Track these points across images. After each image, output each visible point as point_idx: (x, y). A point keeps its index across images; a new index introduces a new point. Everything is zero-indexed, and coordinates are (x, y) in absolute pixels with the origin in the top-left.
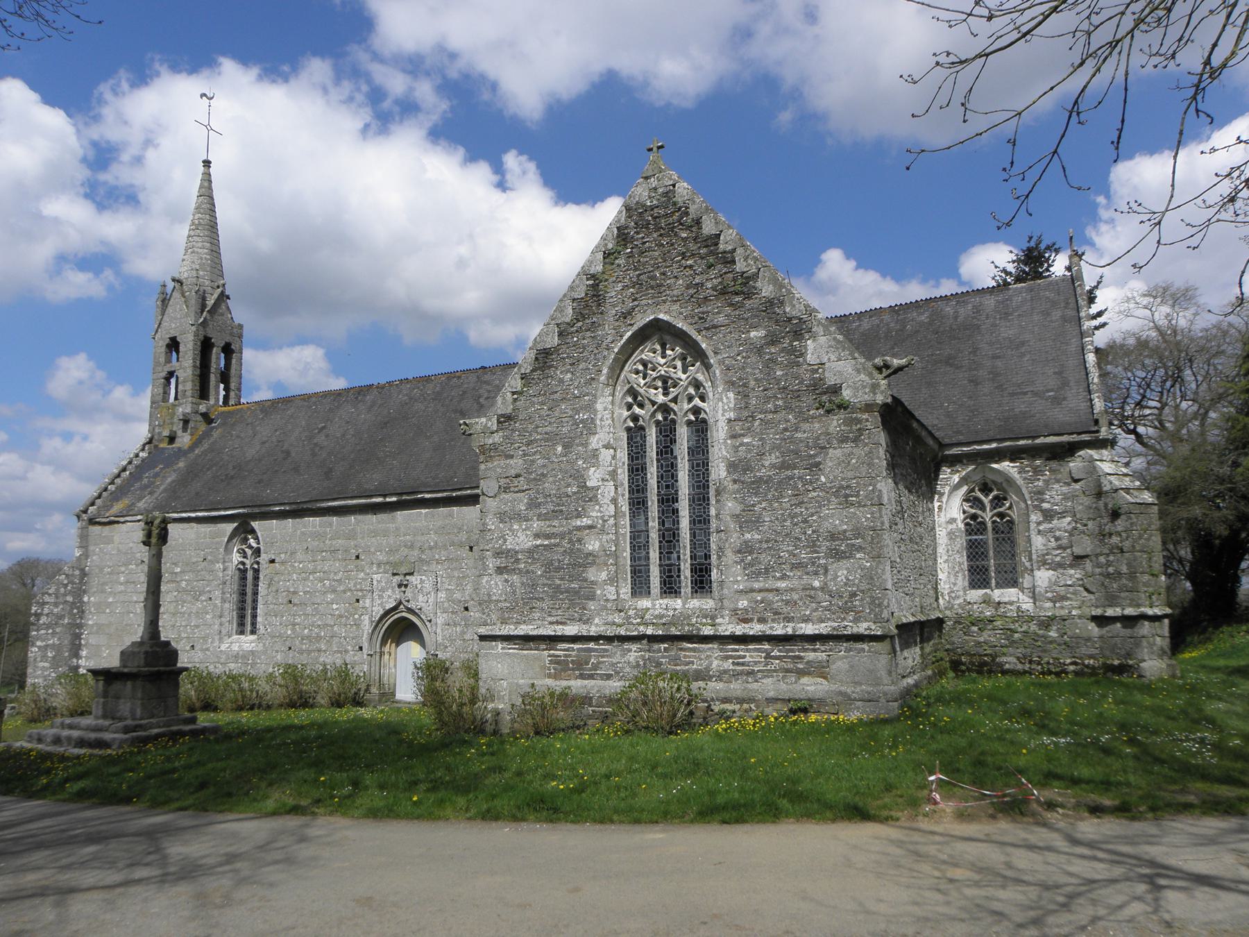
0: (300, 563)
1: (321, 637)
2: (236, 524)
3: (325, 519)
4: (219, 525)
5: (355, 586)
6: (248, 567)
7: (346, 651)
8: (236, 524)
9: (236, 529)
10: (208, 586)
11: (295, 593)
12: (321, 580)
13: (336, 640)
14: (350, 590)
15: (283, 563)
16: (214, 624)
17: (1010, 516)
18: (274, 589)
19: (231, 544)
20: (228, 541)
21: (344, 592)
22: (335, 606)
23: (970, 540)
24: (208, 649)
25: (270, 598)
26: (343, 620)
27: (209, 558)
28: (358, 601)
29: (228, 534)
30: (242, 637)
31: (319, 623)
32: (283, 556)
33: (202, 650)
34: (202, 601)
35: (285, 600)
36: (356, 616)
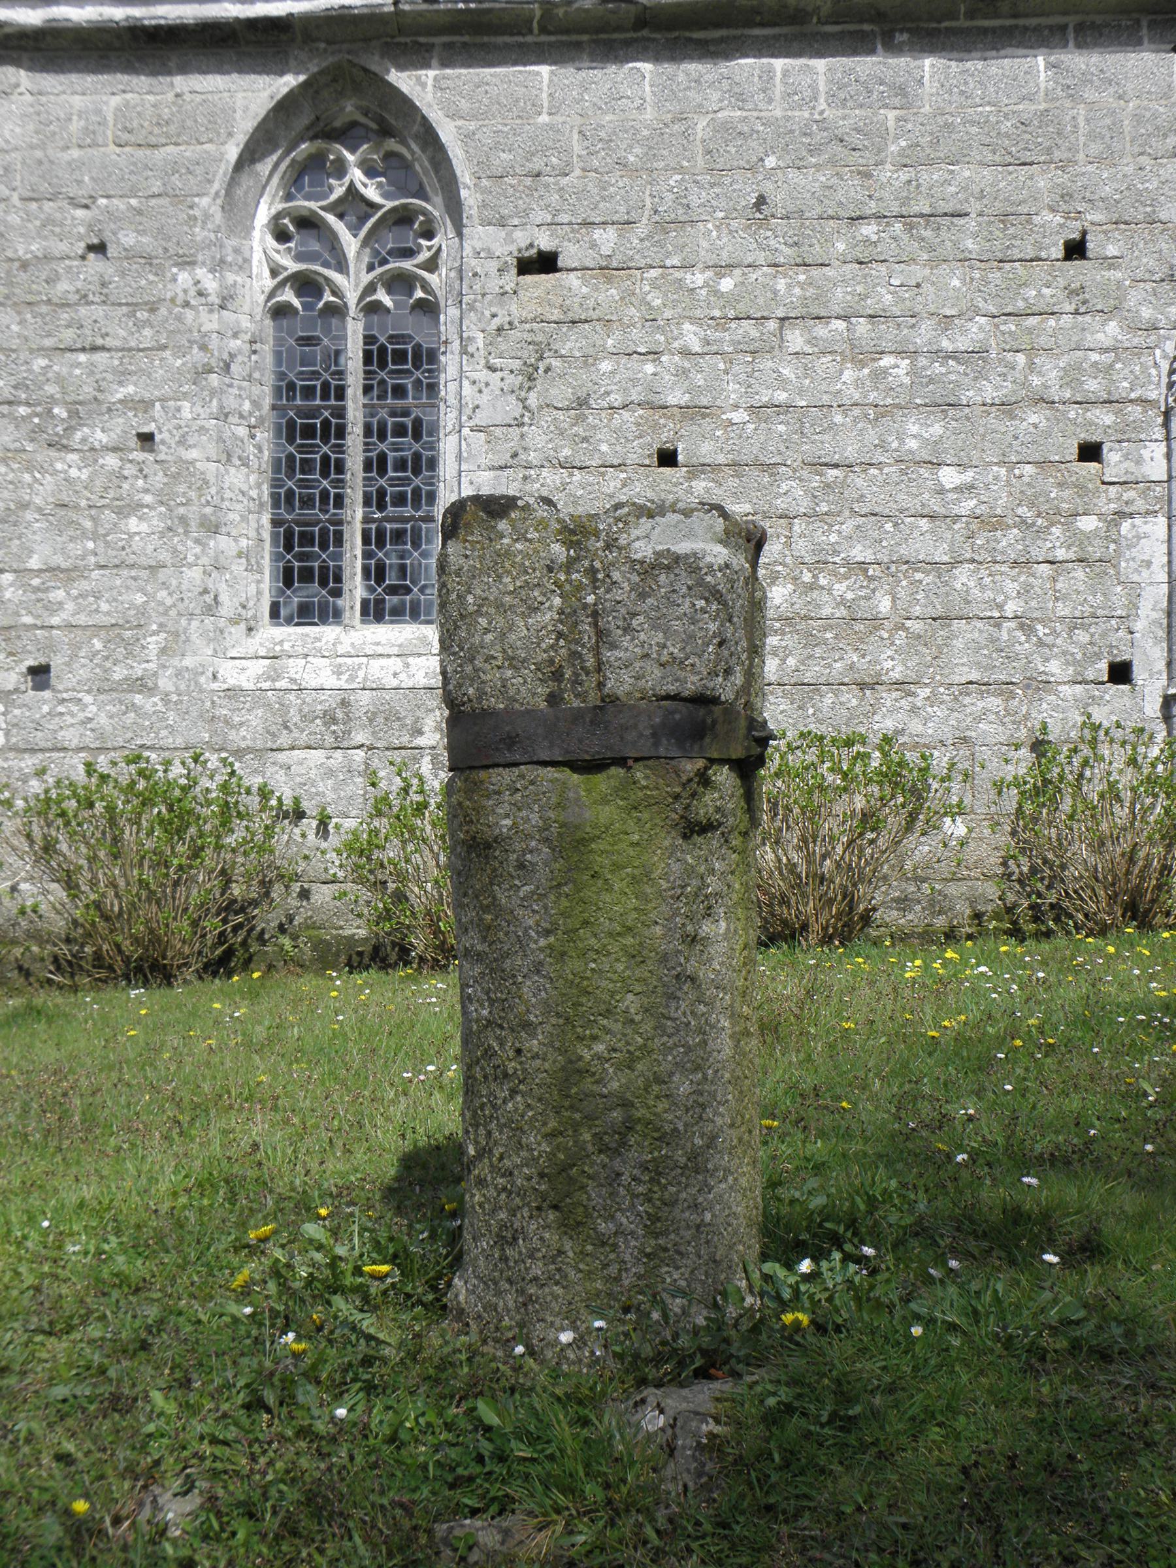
0: (722, 269)
1: (876, 621)
2: (289, 81)
3: (866, 65)
4: (180, 82)
5: (1071, 376)
6: (352, 298)
7: (1039, 685)
8: (289, 81)
9: (284, 108)
10: (123, 376)
11: (694, 412)
12: (858, 355)
13: (966, 634)
14: (1042, 400)
15: (607, 269)
16: (180, 563)
17: (426, 287)
18: (561, 393)
19: (246, 181)
20: (239, 166)
21: (1006, 407)
22: (949, 477)
23: (365, 612)
24: (142, 685)
25: (538, 438)
26: (1009, 541)
27: (128, 238)
28: (1090, 452)
29: (245, 126)
30: (328, 633)
31: (859, 553)
32: (607, 238)
33: (104, 688)
34: (93, 452)
35: (641, 450)
36: (1088, 524)
